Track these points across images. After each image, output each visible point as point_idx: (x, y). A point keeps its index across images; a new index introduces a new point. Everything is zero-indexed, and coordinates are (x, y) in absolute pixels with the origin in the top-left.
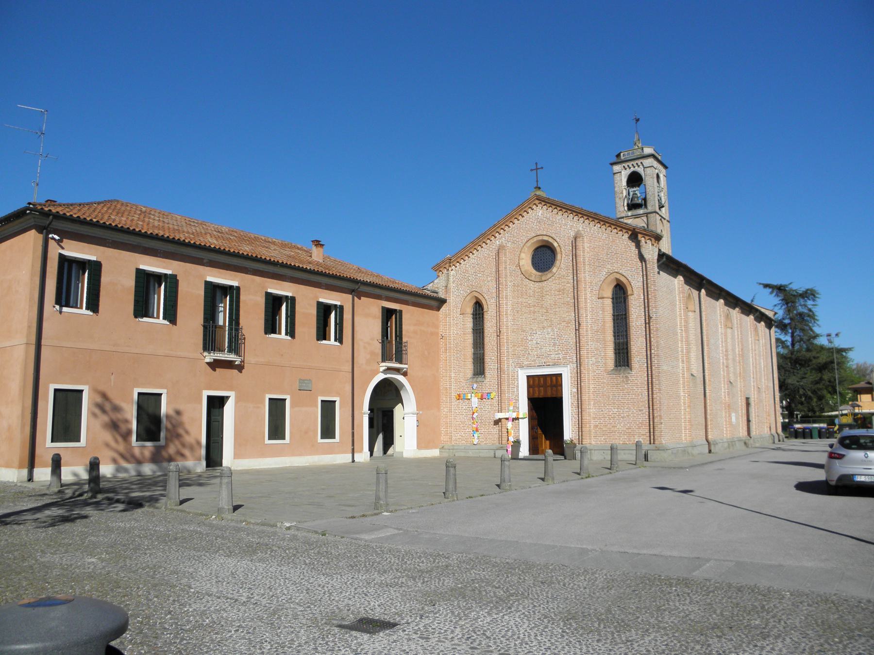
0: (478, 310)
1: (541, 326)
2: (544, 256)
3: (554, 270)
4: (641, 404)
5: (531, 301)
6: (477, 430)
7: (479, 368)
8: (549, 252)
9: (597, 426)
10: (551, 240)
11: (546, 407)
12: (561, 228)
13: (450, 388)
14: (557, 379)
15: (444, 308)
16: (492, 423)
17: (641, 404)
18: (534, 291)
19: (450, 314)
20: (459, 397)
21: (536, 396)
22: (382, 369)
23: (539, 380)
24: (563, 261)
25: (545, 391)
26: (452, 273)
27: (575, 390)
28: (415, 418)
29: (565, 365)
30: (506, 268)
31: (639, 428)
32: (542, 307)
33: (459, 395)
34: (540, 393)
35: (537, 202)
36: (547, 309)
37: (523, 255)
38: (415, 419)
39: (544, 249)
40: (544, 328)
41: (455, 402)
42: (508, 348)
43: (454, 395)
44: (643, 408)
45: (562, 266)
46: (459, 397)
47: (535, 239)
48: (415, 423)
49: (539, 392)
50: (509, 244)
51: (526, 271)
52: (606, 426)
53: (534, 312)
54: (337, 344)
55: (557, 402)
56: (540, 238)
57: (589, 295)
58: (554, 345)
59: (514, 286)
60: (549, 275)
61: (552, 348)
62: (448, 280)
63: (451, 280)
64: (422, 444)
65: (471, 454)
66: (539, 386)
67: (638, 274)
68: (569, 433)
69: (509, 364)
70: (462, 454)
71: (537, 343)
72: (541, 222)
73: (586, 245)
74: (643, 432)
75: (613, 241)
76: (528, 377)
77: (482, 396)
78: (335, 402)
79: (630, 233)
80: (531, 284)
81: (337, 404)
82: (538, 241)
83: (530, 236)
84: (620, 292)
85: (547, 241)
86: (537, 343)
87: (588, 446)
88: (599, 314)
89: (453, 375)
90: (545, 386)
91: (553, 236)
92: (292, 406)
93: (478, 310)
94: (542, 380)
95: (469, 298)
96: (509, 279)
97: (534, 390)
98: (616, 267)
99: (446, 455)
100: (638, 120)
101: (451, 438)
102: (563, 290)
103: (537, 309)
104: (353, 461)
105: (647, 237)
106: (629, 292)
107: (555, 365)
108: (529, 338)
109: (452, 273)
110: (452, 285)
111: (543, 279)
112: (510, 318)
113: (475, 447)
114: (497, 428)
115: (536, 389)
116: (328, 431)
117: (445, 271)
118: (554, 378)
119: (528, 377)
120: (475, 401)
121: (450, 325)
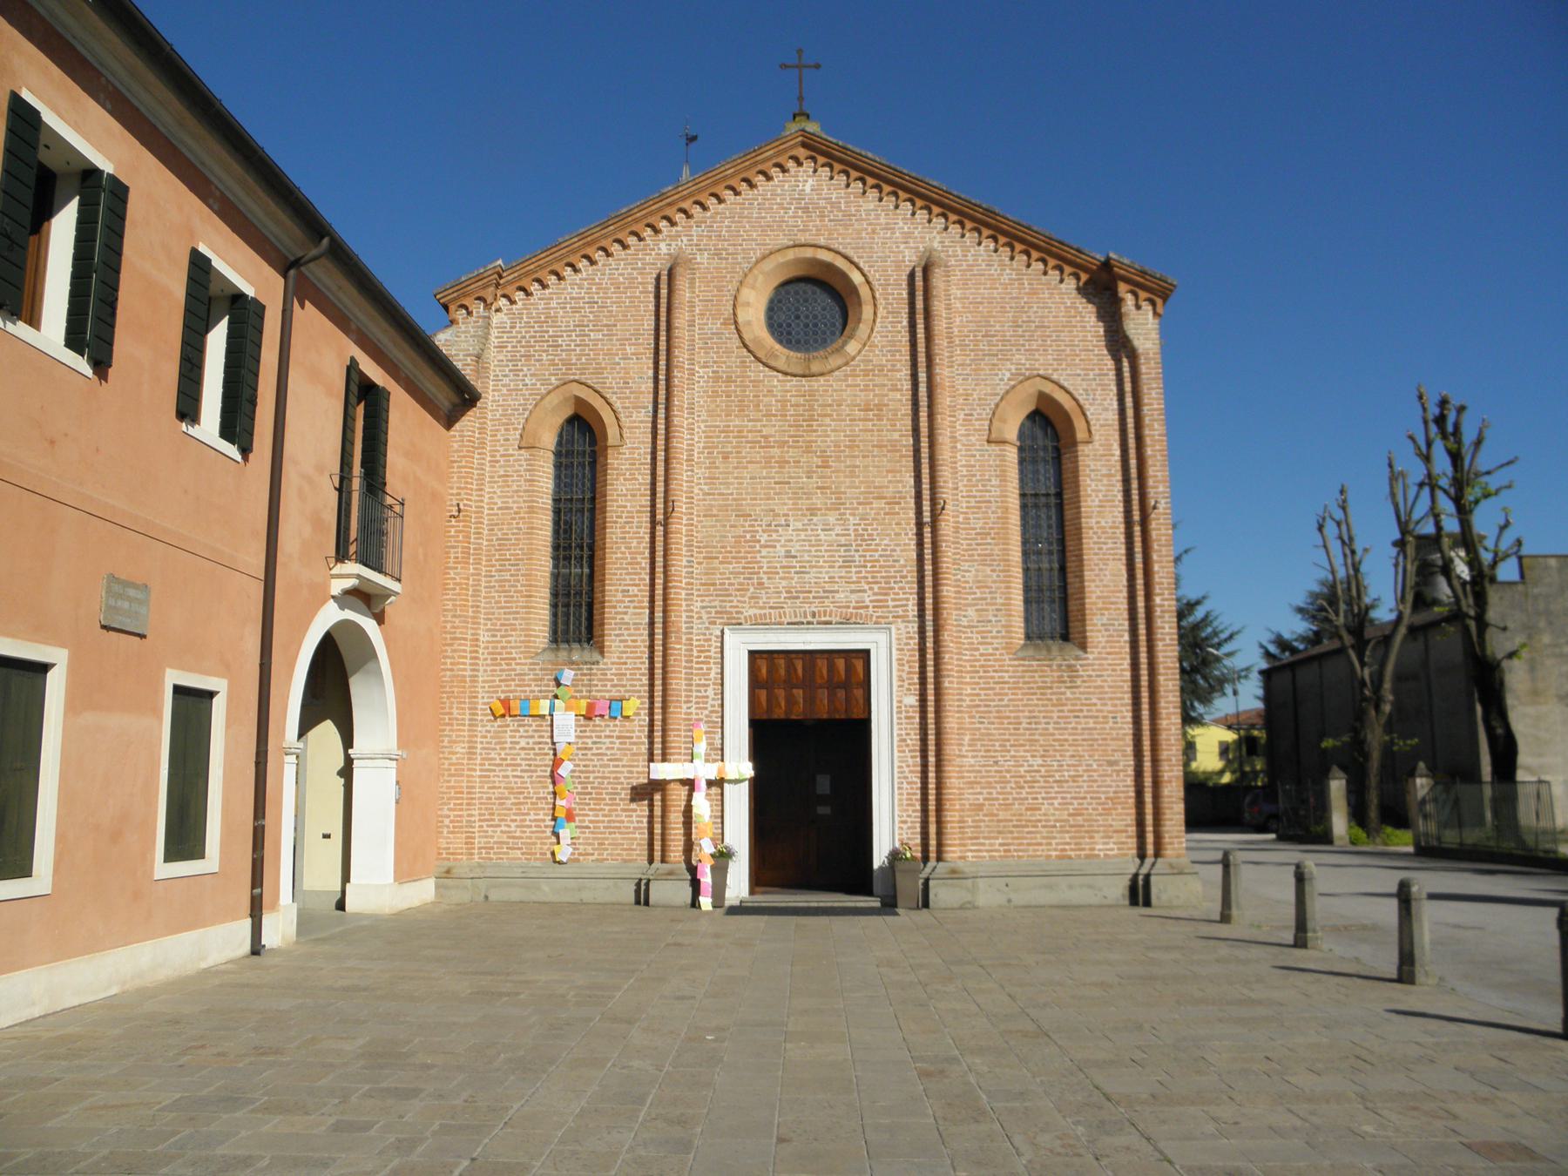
0: (582, 441)
1: (804, 503)
2: (816, 304)
3: (852, 347)
4: (1113, 745)
5: (772, 429)
6: (570, 817)
7: (577, 616)
8: (825, 300)
9: (980, 807)
10: (840, 263)
11: (810, 746)
12: (880, 237)
14: (849, 669)
15: (468, 422)
17: (1113, 745)
18: (784, 402)
21: (779, 713)
22: (337, 587)
23: (790, 667)
24: (881, 332)
25: (810, 700)
26: (496, 319)
27: (913, 700)
29: (880, 624)
30: (692, 324)
31: (1107, 812)
32: (808, 450)
33: (506, 703)
34: (792, 705)
35: (802, 153)
37: (747, 294)
38: (392, 775)
39: (809, 288)
40: (813, 511)
42: (690, 564)
43: (485, 700)
44: (1117, 756)
45: (877, 338)
46: (507, 710)
47: (791, 255)
49: (791, 701)
50: (702, 259)
52: (1007, 807)
53: (783, 463)
55: (850, 739)
56: (809, 253)
57: (961, 430)
58: (848, 562)
59: (716, 378)
60: (834, 361)
62: (486, 337)
63: (493, 340)
64: (405, 872)
65: (547, 892)
66: (789, 684)
67: (1104, 387)
68: (890, 827)
70: (515, 895)
71: (789, 555)
72: (804, 206)
73: (956, 292)
74: (1118, 825)
75: (1034, 292)
76: (753, 654)
77: (591, 707)
79: (1084, 277)
80: (776, 380)
82: (799, 261)
84: (1049, 433)
85: (830, 267)
86: (789, 555)
87: (960, 864)
88: (985, 486)
89: (484, 637)
90: (809, 683)
91: (850, 253)
92: (73, 706)
93: (582, 441)
94: (799, 665)
95: (554, 399)
96: (700, 357)
97: (771, 698)
98: (1044, 363)
99: (460, 896)
100: (692, 139)
101: (469, 843)
102: (879, 407)
103: (792, 453)
105: (1143, 294)
106: (1081, 434)
107: (846, 622)
108: (764, 538)
109: (496, 319)
110: (492, 355)
111: (815, 367)
112: (700, 472)
114: (642, 809)
115: (781, 694)
116: (185, 837)
118: (841, 663)
119: (753, 654)
120: (566, 724)
121: (481, 478)
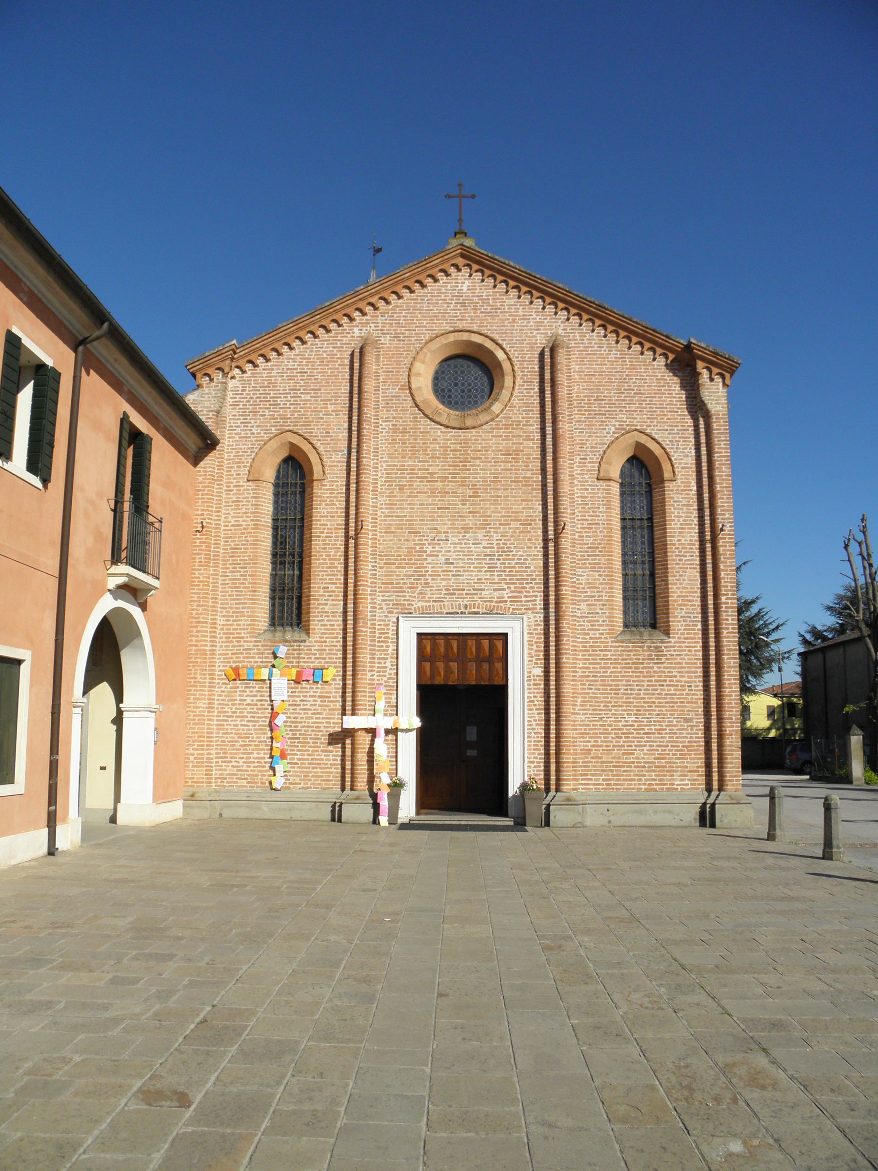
0: (294, 476)
1: (459, 524)
2: (469, 375)
3: (496, 408)
4: (689, 707)
7: (289, 606)
11: (462, 708)
12: (519, 326)
13: (213, 653)
14: (492, 646)
16: (324, 739)
17: (689, 707)
19: (220, 478)
20: (237, 675)
21: (439, 680)
23: (448, 646)
25: (463, 670)
26: (231, 384)
28: (150, 723)
29: (515, 614)
30: (377, 389)
31: (683, 757)
33: (236, 670)
34: (448, 674)
35: (461, 261)
36: (475, 489)
37: (418, 367)
39: (465, 363)
40: (466, 529)
41: (223, 688)
43: (220, 667)
44: (692, 715)
45: (515, 401)
46: (237, 675)
47: (452, 338)
48: (151, 735)
49: (448, 670)
50: (385, 340)
51: (424, 401)
52: (608, 751)
53: (444, 493)
54: (36, 481)
55: (495, 697)
56: (465, 337)
58: (491, 569)
59: (395, 429)
60: (484, 417)
61: (484, 576)
63: (229, 400)
64: (161, 795)
65: (266, 811)
66: (447, 658)
68: (521, 766)
69: (374, 604)
70: (243, 813)
72: (460, 302)
75: (633, 367)
77: (299, 674)
78: (19, 662)
79: (671, 356)
81: (25, 671)
82: (457, 343)
83: (438, 330)
84: (643, 473)
85: (480, 347)
87: (573, 794)
88: (595, 512)
89: (220, 621)
91: (496, 337)
93: (294, 476)
96: (383, 414)
99: (200, 814)
100: (379, 250)
102: (517, 452)
104: (52, 851)
106: (667, 475)
107: (490, 613)
108: (429, 549)
112: (382, 499)
113: (275, 795)
114: (337, 750)
115: (441, 665)
117: (218, 376)
118: (486, 643)
120: (281, 686)
